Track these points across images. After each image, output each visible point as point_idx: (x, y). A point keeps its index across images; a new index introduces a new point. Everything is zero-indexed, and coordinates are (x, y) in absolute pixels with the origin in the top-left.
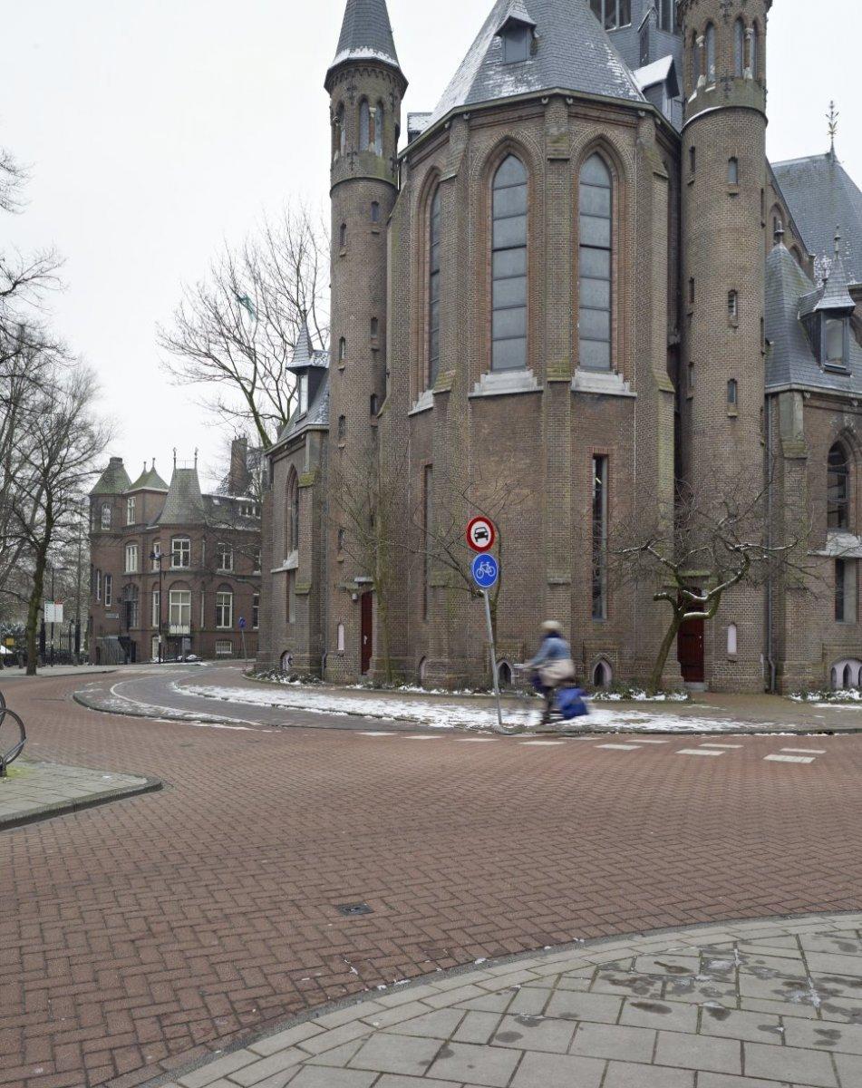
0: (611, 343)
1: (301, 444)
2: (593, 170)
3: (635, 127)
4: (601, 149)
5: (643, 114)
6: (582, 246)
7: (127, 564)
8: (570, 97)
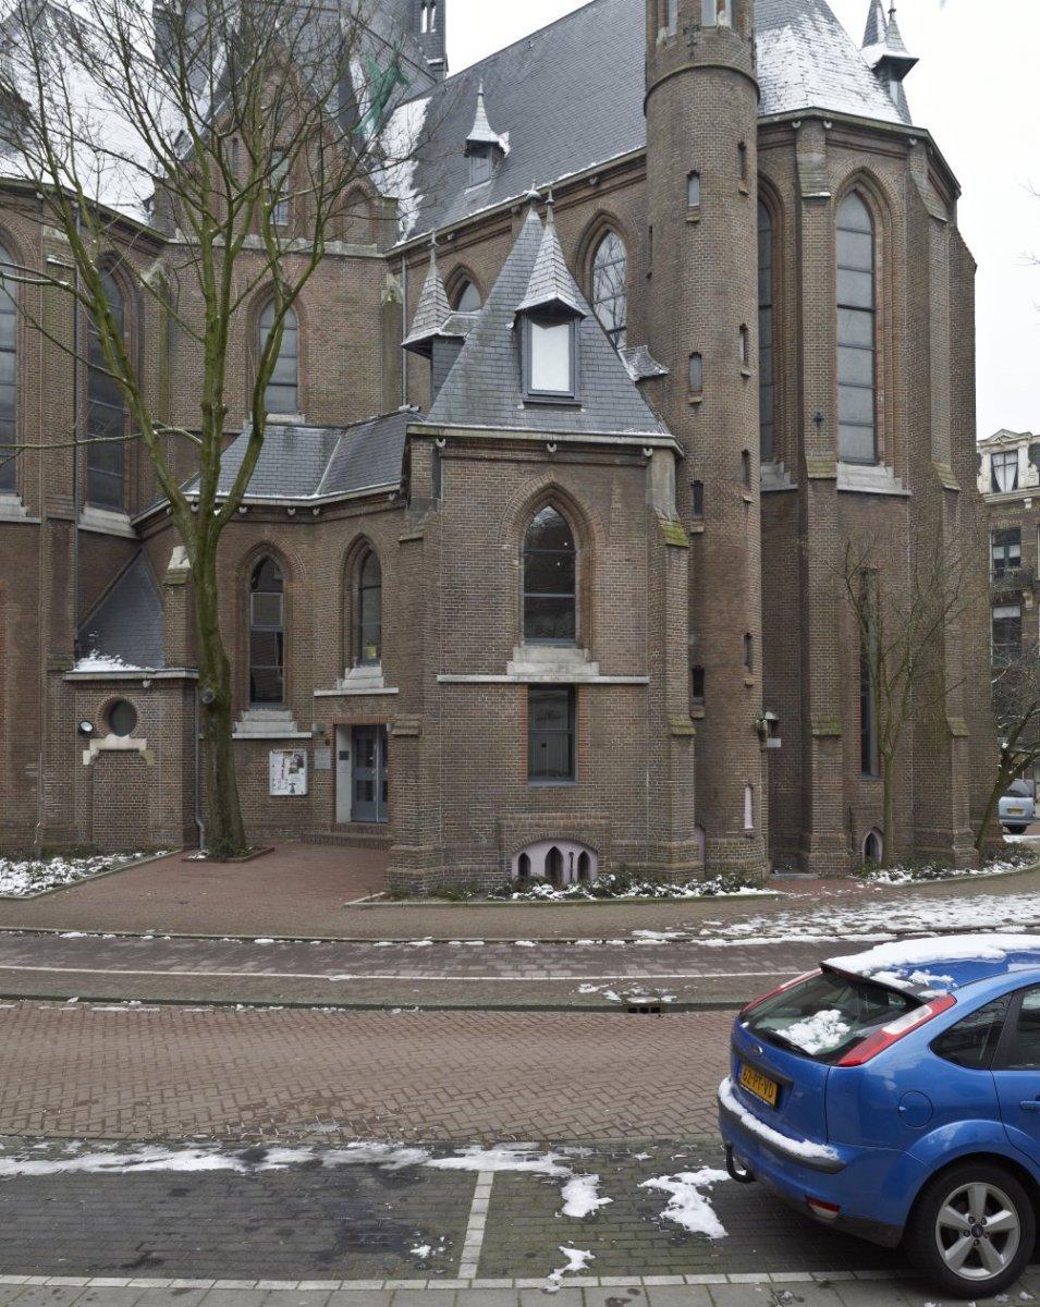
0: (873, 237)
1: (423, 256)
2: (854, 214)
3: (903, 157)
5: (913, 142)
7: (265, 502)
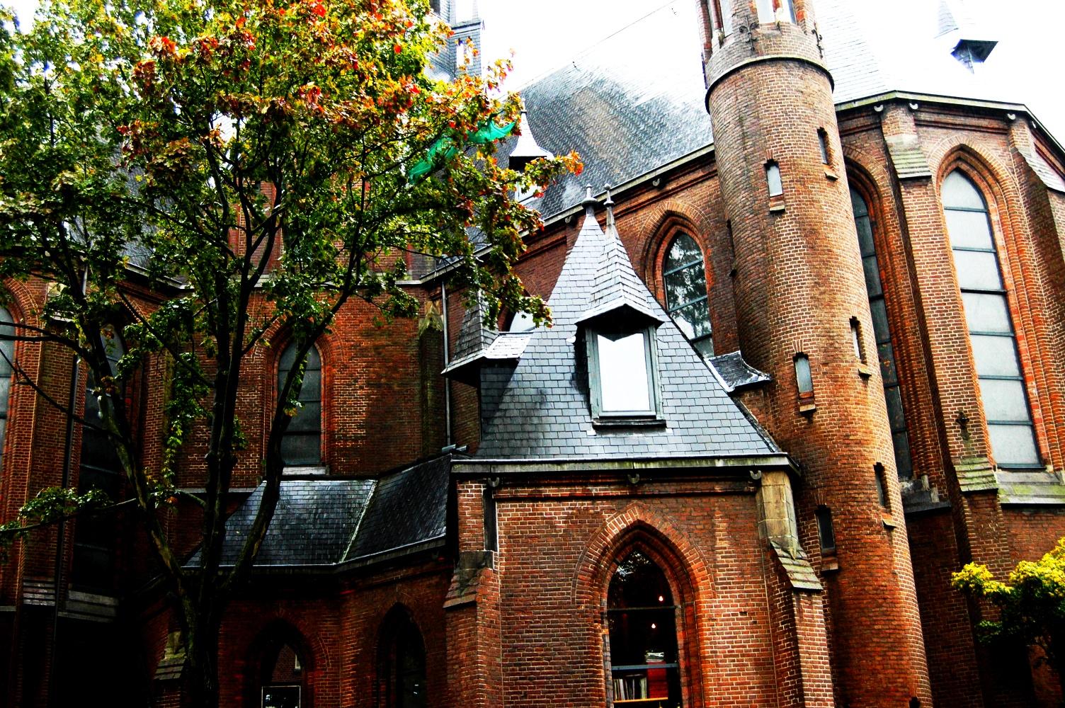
2: (957, 191)
4: (964, 163)
5: (1012, 117)
6: (963, 291)
8: (914, 102)
